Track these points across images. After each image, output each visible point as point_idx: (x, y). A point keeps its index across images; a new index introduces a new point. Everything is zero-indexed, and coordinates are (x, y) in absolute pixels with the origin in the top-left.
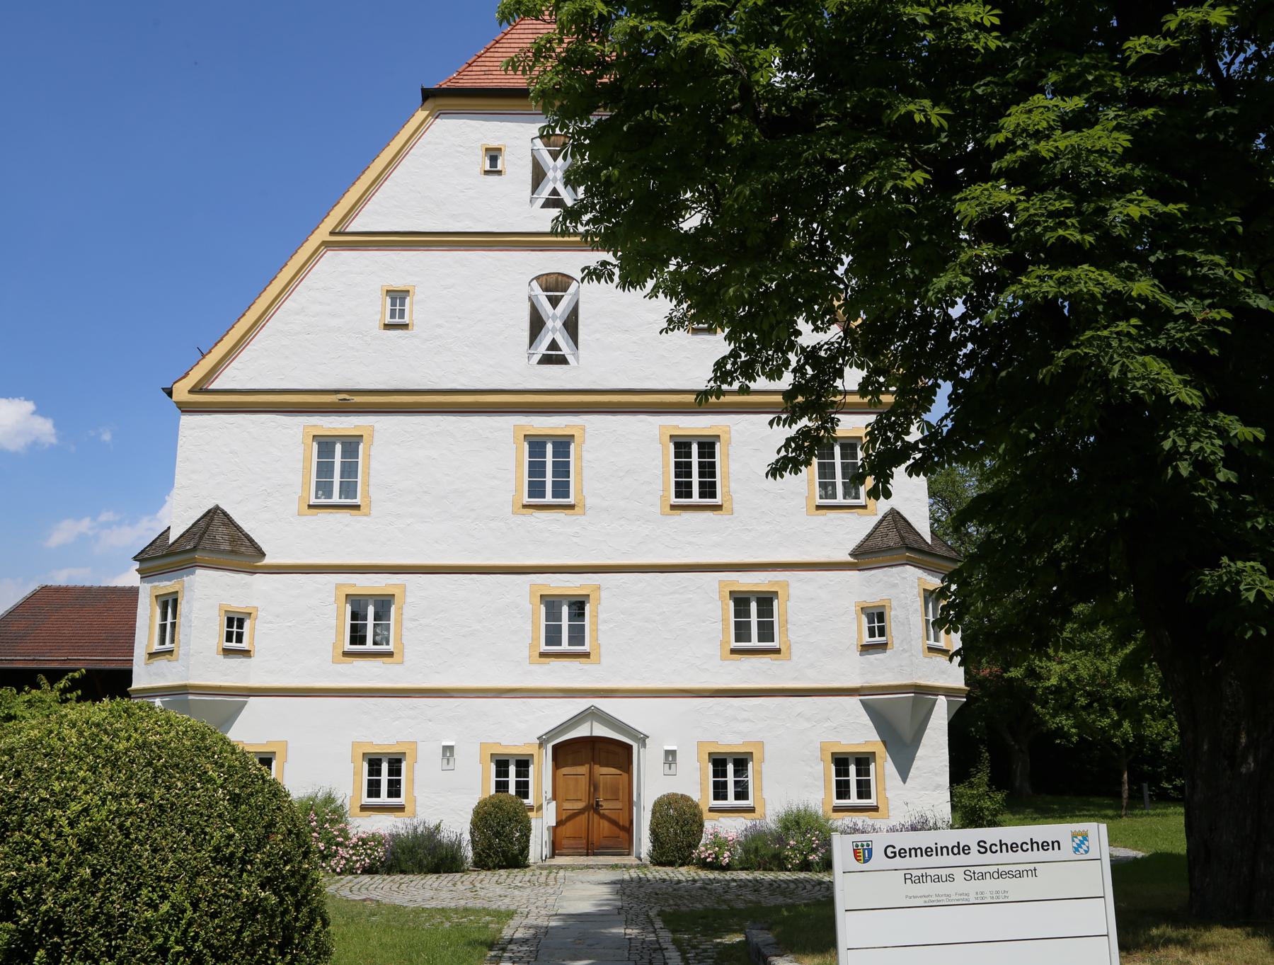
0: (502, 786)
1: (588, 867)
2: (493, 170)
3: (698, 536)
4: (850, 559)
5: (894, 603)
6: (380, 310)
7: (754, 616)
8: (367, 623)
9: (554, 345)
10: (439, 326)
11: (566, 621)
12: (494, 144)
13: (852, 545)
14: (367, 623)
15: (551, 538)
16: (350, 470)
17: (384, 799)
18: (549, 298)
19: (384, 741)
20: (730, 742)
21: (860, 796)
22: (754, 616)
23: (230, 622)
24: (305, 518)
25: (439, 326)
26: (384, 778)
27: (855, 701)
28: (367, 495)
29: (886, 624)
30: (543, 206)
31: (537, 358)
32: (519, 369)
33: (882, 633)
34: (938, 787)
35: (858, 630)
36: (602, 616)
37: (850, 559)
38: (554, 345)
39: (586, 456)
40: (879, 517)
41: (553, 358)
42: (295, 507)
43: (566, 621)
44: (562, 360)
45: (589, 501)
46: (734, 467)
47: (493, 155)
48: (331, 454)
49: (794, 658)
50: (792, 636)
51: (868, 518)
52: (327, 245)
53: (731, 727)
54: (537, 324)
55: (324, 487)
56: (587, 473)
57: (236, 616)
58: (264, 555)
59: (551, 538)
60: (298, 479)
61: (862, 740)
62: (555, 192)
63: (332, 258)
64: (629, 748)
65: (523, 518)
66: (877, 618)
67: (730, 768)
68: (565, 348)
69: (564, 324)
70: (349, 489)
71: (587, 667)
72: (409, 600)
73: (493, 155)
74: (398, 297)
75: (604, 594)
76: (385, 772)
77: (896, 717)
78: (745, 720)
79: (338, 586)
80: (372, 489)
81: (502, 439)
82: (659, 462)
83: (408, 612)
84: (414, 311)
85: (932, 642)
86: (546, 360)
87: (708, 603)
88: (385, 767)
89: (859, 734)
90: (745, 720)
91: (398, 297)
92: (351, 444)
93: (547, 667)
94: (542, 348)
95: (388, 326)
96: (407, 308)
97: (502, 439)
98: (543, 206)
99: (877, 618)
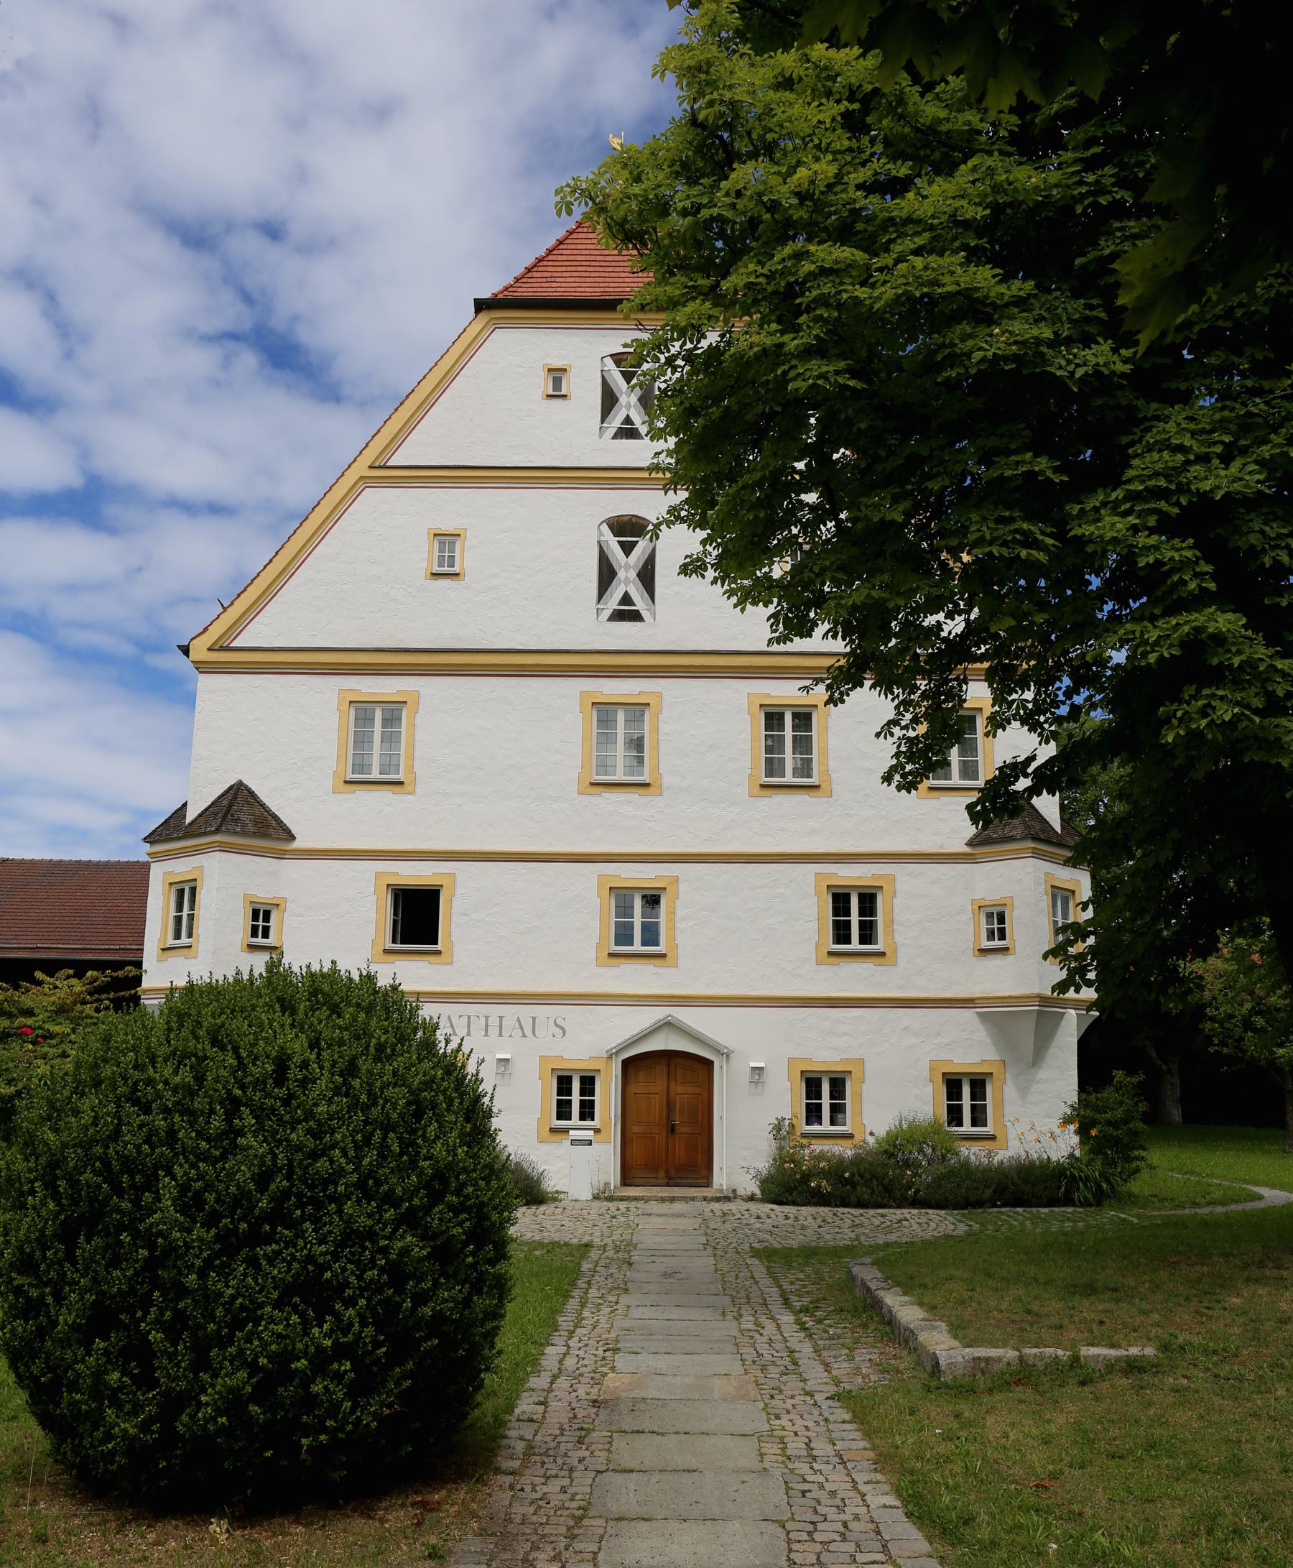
1: (636, 1199)
2: (557, 394)
3: (791, 822)
4: (967, 850)
5: (1016, 902)
6: (422, 556)
7: (854, 917)
9: (626, 599)
11: (638, 921)
15: (624, 824)
16: (804, 745)
18: (622, 544)
20: (825, 1057)
21: (974, 1125)
22: (854, 917)
23: (255, 914)
26: (966, 1102)
27: (968, 1015)
28: (411, 769)
29: (273, 923)
30: (615, 437)
35: (973, 931)
36: (680, 913)
37: (967, 850)
38: (626, 599)
39: (663, 728)
41: (627, 614)
42: (329, 784)
43: (638, 921)
44: (636, 616)
45: (666, 781)
46: (833, 742)
47: (557, 375)
49: (901, 963)
50: (898, 939)
53: (826, 1042)
54: (607, 574)
55: (773, 767)
57: (995, 910)
58: (294, 838)
61: (977, 1059)
62: (628, 420)
64: (709, 1064)
65: (589, 798)
67: (825, 1091)
68: (640, 603)
69: (638, 575)
70: (805, 768)
72: (458, 891)
73: (557, 375)
74: (447, 541)
75: (682, 887)
77: (1021, 1023)
78: (844, 1034)
80: (417, 763)
82: (747, 735)
84: (467, 559)
86: (619, 616)
87: (802, 905)
88: (966, 1091)
89: (969, 1046)
90: (844, 1034)
91: (447, 541)
92: (394, 711)
93: (616, 970)
94: (613, 602)
95: (436, 575)
96: (457, 555)
98: (615, 437)
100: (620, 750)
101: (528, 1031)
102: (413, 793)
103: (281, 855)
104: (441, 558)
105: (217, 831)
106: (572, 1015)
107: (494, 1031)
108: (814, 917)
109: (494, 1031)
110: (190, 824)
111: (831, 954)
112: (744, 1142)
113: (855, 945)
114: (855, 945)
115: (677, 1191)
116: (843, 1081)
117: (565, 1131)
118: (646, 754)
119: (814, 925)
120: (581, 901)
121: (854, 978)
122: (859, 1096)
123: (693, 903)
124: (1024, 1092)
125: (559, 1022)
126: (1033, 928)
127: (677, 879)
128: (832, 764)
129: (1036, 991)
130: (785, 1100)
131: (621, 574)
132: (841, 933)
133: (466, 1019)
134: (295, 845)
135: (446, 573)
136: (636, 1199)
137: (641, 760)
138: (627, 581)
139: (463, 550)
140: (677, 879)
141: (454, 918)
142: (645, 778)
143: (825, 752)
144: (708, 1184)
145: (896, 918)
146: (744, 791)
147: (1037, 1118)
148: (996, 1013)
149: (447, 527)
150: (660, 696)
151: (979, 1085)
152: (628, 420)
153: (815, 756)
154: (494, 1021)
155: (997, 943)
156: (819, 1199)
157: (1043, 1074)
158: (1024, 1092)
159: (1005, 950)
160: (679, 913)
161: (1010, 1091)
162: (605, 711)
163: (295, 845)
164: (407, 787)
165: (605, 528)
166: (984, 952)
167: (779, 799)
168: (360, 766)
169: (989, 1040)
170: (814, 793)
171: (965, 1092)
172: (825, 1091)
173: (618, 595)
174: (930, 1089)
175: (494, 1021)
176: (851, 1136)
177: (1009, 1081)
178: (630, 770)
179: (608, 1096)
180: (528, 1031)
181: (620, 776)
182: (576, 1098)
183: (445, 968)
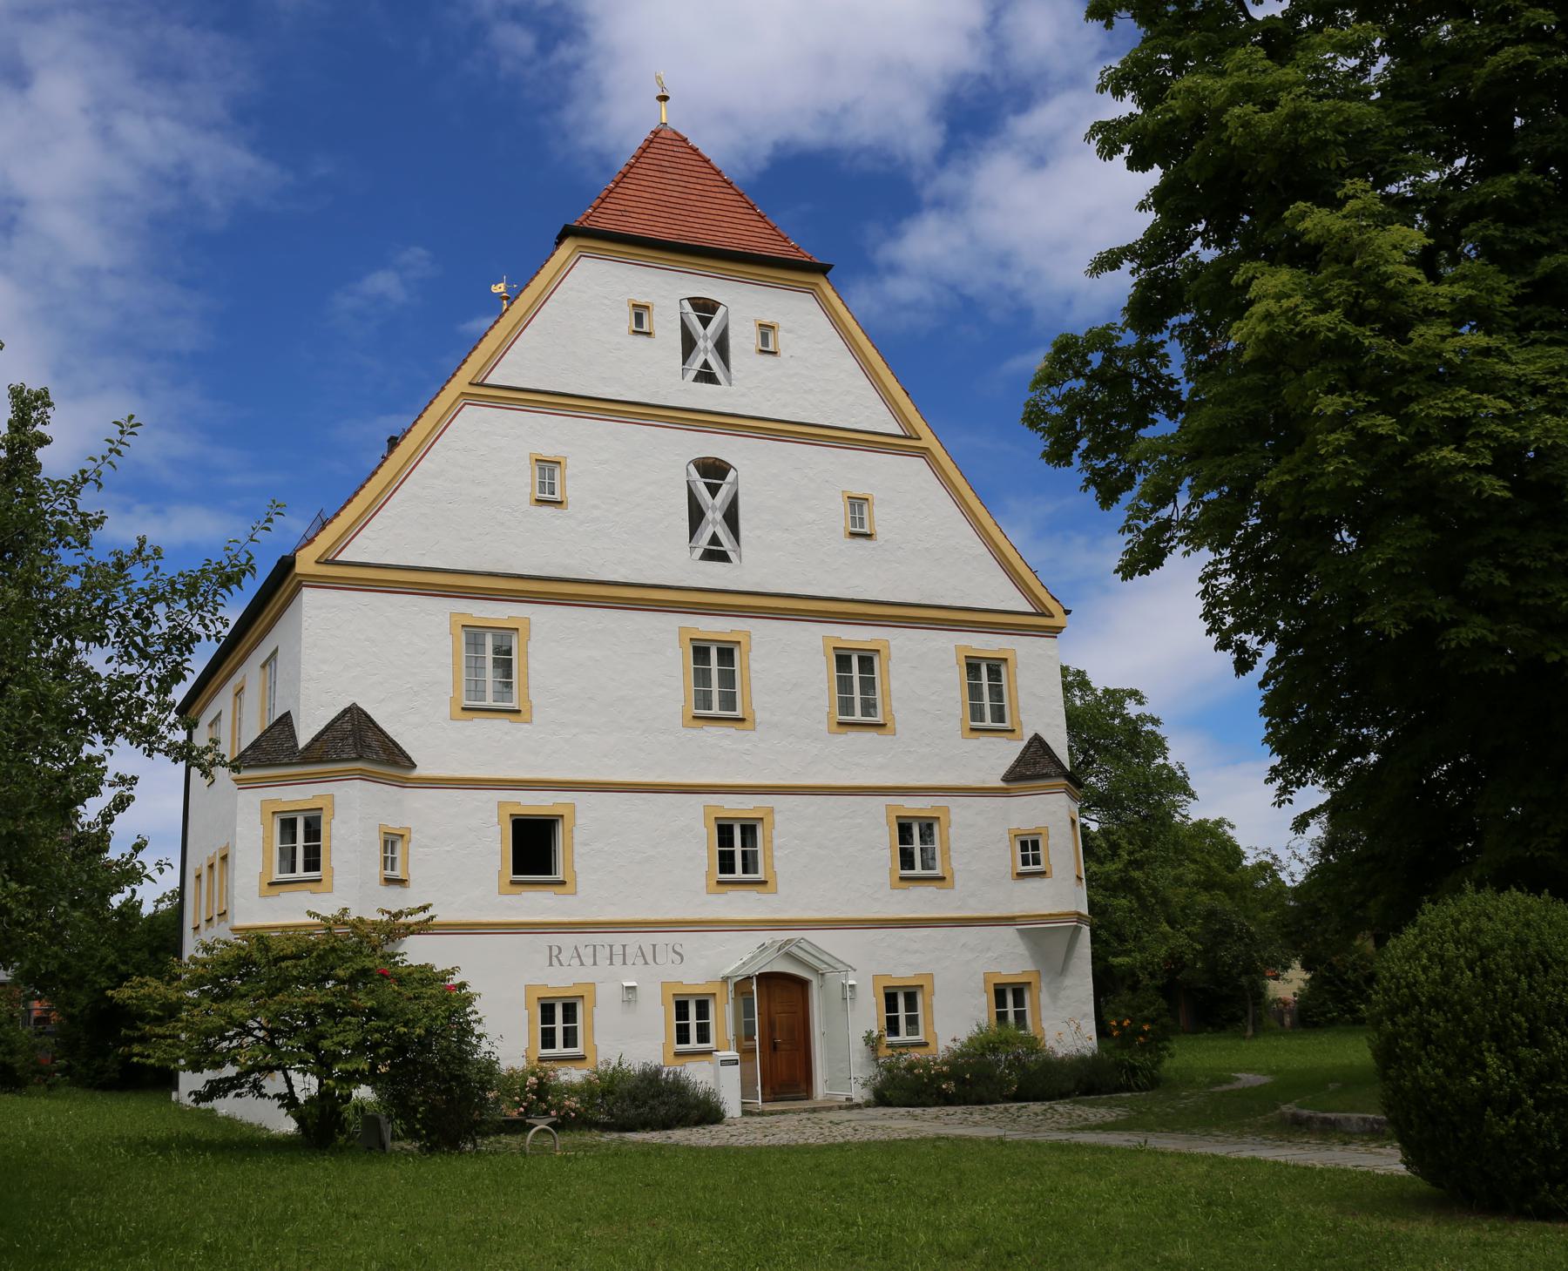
0: (1002, 1017)
1: (783, 1112)
3: (861, 758)
4: (1003, 785)
6: (525, 483)
7: (914, 843)
8: (534, 847)
9: (715, 540)
10: (595, 507)
11: (736, 849)
12: (642, 301)
13: (1003, 770)
14: (534, 847)
15: (721, 755)
17: (694, 1044)
19: (559, 981)
20: (902, 973)
23: (1024, 845)
24: (459, 724)
25: (595, 507)
27: (1009, 932)
29: (1041, 852)
30: (695, 380)
31: (699, 552)
32: (679, 563)
33: (1037, 861)
34: (1085, 1016)
35: (1009, 857)
37: (1003, 785)
38: (715, 540)
39: (754, 666)
40: (1025, 743)
41: (715, 554)
42: (446, 710)
43: (736, 849)
44: (723, 557)
45: (759, 716)
47: (640, 313)
48: (707, 660)
49: (957, 886)
50: (954, 864)
51: (1015, 743)
52: (466, 398)
53: (900, 957)
54: (696, 515)
56: (756, 685)
57: (1029, 839)
58: (414, 766)
59: (721, 755)
60: (447, 676)
62: (706, 364)
63: (472, 415)
64: (803, 984)
65: (694, 732)
66: (1030, 848)
68: (727, 544)
69: (724, 517)
70: (729, 701)
71: (764, 897)
72: (578, 822)
73: (640, 313)
74: (547, 467)
75: (777, 818)
76: (558, 1017)
78: (916, 952)
79: (500, 804)
81: (662, 643)
82: (824, 675)
83: (579, 836)
84: (571, 486)
85: (389, 872)
86: (709, 555)
87: (873, 827)
90: (916, 952)
91: (547, 467)
93: (724, 897)
97: (662, 643)
98: (695, 380)
99: (1030, 848)
100: (490, 674)
101: (650, 958)
102: (530, 722)
103: (404, 783)
104: (542, 484)
105: (359, 758)
106: (688, 941)
107: (618, 960)
108: (498, 846)
109: (618, 960)
110: (308, 747)
111: (719, 883)
112: (842, 1056)
113: (300, 873)
114: (738, 874)
115: (778, 1106)
116: (574, 1005)
117: (709, 1053)
118: (515, 679)
119: (887, 853)
120: (689, 832)
121: (920, 901)
122: (929, 1008)
123: (788, 835)
124: (1054, 997)
125: (678, 948)
126: (1063, 854)
127: (772, 810)
128: (894, 704)
129: (1073, 909)
130: (868, 1015)
131: (709, 515)
132: (726, 864)
133: (591, 949)
134: (416, 773)
135: (548, 500)
136: (783, 1112)
137: (509, 685)
138: (714, 522)
139: (563, 479)
140: (772, 810)
141: (572, 849)
142: (514, 705)
143: (887, 694)
144: (808, 1094)
145: (953, 846)
146: (824, 727)
147: (1067, 1023)
148: (1038, 932)
149: (548, 453)
150: (748, 634)
151: (1019, 992)
152: (706, 364)
153: (738, 689)
154: (618, 949)
155: (1031, 868)
156: (947, 1100)
157: (1068, 982)
158: (1054, 997)
159: (1042, 874)
160: (776, 842)
161: (1044, 998)
162: (474, 635)
163: (416, 773)
164: (524, 715)
165: (692, 468)
166: (1021, 875)
167: (985, 739)
168: (476, 689)
169: (1026, 953)
170: (881, 731)
171: (1009, 995)
172: (901, 1002)
173: (707, 536)
174: (984, 999)
175: (618, 949)
176: (582, 1058)
177: (1044, 989)
178: (499, 696)
179: (723, 1019)
180: (650, 958)
181: (489, 702)
182: (559, 1025)
183: (569, 898)
